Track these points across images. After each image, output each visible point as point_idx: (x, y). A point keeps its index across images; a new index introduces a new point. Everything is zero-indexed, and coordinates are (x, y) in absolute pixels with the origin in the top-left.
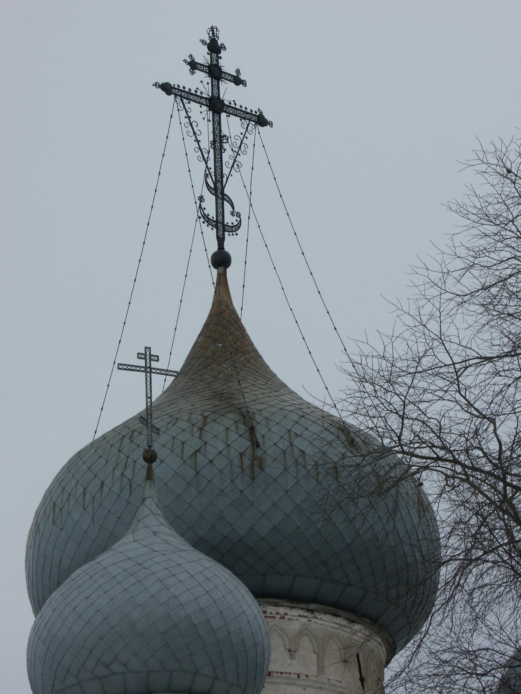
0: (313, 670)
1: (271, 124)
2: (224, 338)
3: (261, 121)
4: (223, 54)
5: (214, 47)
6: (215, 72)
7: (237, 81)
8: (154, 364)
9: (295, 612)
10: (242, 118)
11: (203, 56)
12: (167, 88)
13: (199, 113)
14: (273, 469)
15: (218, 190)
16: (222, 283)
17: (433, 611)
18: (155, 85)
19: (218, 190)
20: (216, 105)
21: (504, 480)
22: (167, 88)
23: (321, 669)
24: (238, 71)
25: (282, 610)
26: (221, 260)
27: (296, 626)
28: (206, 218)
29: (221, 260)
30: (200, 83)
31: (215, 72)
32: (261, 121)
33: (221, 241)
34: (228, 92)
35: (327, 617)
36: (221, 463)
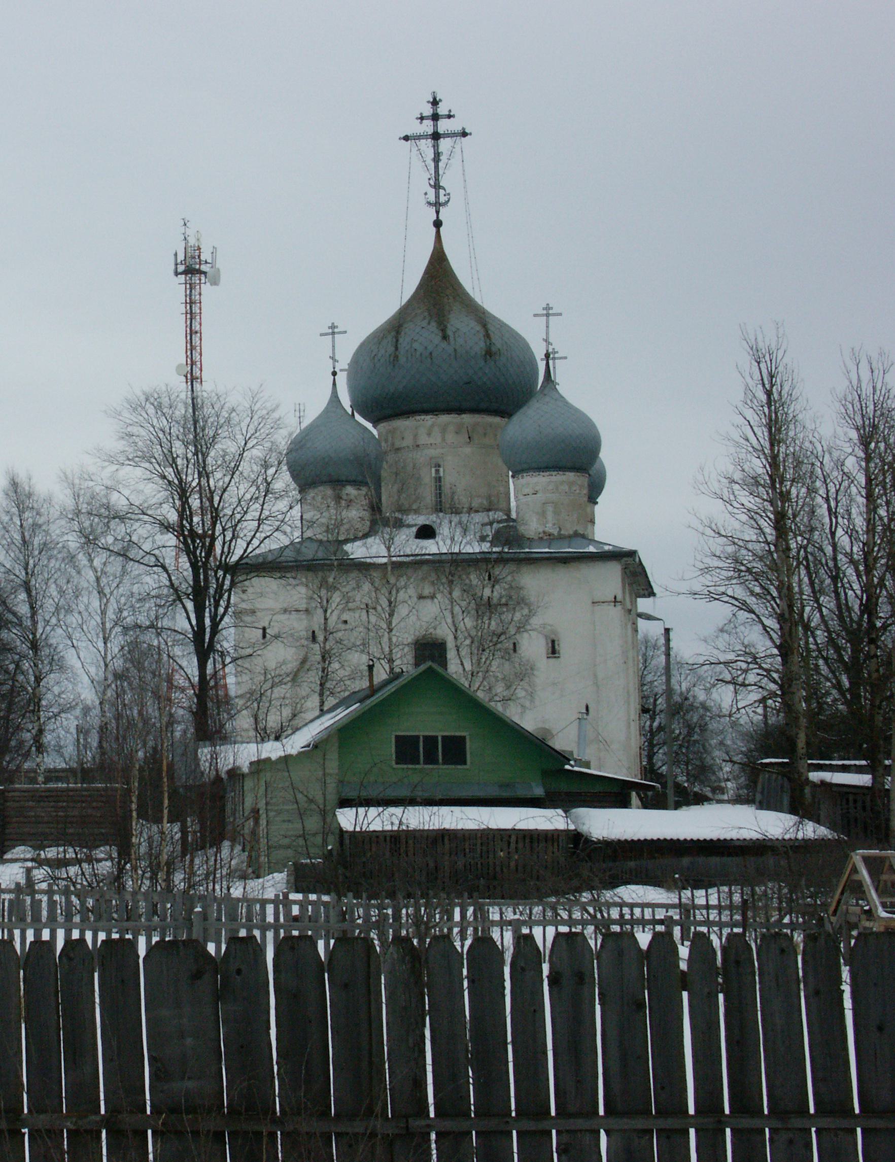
0: (439, 440)
2: (439, 260)
9: (428, 417)
12: (406, 138)
14: (402, 360)
15: (437, 186)
18: (400, 139)
19: (437, 186)
22: (406, 138)
23: (443, 439)
25: (423, 417)
26: (438, 224)
27: (430, 423)
28: (429, 203)
29: (438, 224)
32: (436, 128)
33: (438, 212)
35: (443, 416)
36: (382, 360)
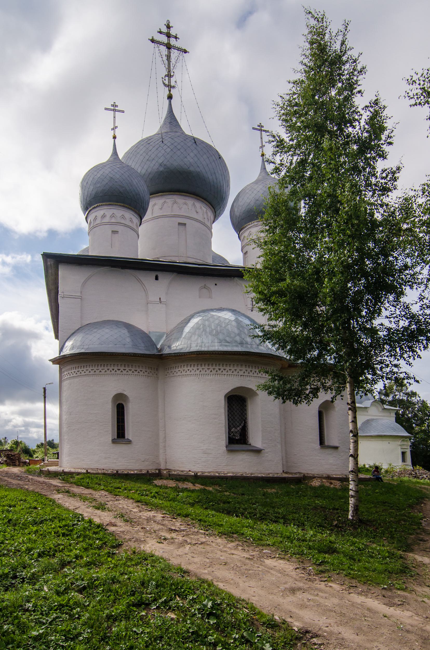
1: (189, 52)
3: (185, 52)
4: (171, 29)
5: (168, 27)
6: (169, 36)
7: (176, 38)
8: (262, 128)
10: (178, 50)
11: (165, 30)
13: (164, 49)
16: (170, 105)
17: (97, 495)
20: (169, 47)
21: (409, 209)
24: (160, 29)
26: (170, 97)
29: (170, 97)
30: (164, 39)
31: (169, 36)
33: (170, 91)
34: (173, 42)
